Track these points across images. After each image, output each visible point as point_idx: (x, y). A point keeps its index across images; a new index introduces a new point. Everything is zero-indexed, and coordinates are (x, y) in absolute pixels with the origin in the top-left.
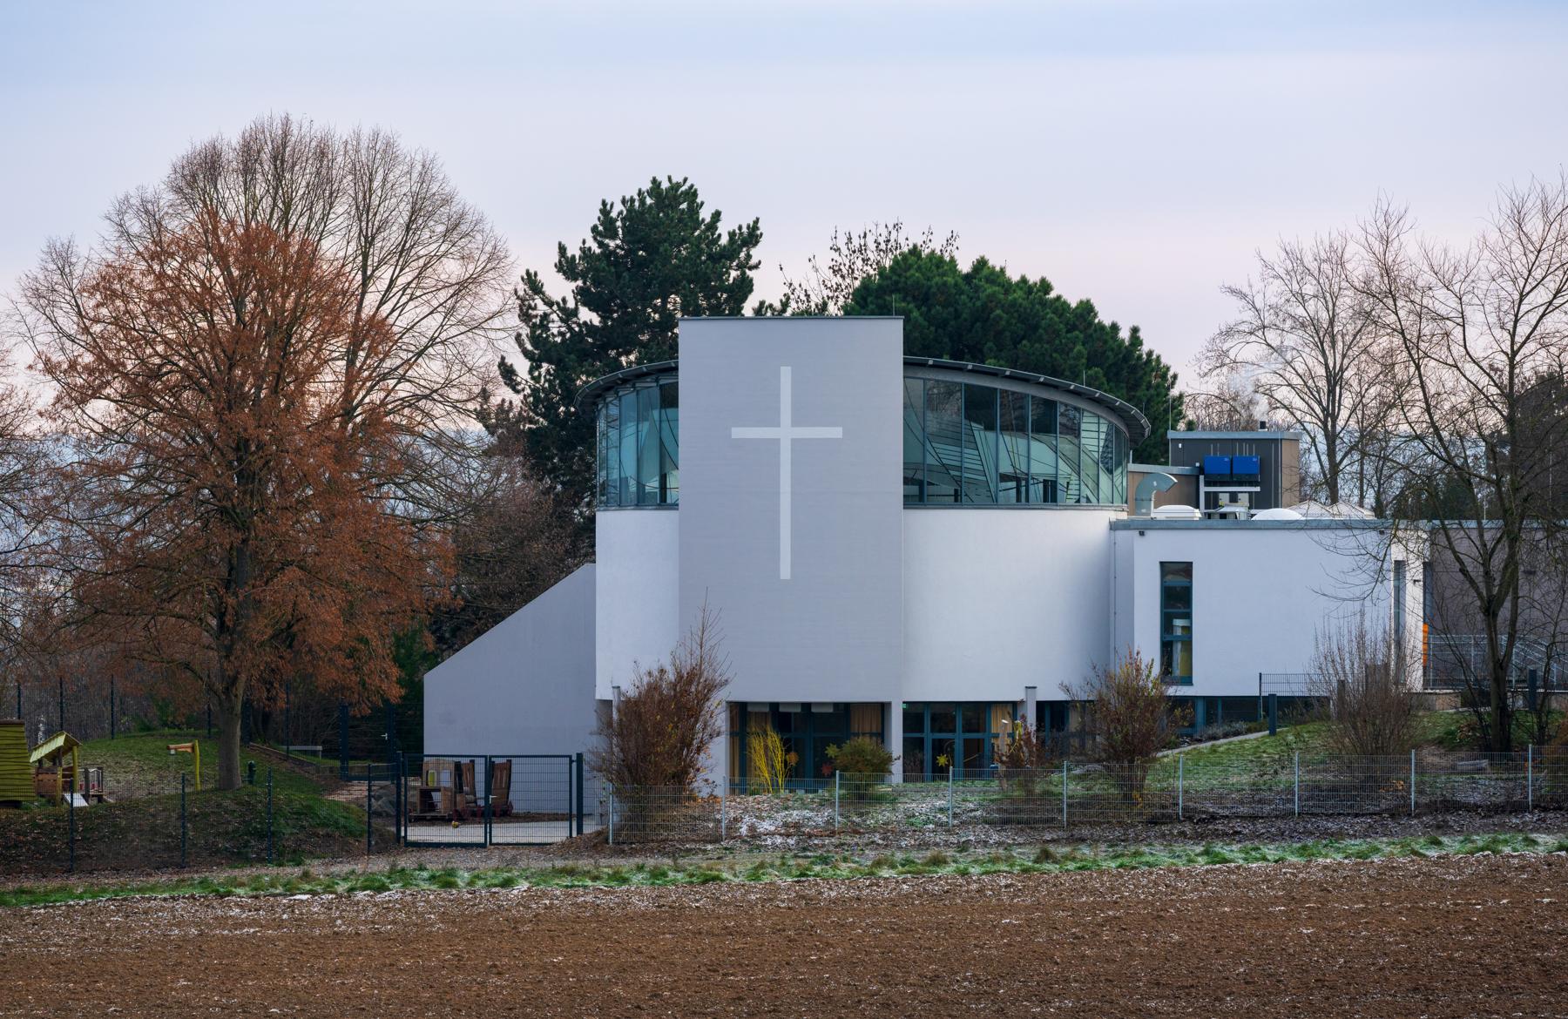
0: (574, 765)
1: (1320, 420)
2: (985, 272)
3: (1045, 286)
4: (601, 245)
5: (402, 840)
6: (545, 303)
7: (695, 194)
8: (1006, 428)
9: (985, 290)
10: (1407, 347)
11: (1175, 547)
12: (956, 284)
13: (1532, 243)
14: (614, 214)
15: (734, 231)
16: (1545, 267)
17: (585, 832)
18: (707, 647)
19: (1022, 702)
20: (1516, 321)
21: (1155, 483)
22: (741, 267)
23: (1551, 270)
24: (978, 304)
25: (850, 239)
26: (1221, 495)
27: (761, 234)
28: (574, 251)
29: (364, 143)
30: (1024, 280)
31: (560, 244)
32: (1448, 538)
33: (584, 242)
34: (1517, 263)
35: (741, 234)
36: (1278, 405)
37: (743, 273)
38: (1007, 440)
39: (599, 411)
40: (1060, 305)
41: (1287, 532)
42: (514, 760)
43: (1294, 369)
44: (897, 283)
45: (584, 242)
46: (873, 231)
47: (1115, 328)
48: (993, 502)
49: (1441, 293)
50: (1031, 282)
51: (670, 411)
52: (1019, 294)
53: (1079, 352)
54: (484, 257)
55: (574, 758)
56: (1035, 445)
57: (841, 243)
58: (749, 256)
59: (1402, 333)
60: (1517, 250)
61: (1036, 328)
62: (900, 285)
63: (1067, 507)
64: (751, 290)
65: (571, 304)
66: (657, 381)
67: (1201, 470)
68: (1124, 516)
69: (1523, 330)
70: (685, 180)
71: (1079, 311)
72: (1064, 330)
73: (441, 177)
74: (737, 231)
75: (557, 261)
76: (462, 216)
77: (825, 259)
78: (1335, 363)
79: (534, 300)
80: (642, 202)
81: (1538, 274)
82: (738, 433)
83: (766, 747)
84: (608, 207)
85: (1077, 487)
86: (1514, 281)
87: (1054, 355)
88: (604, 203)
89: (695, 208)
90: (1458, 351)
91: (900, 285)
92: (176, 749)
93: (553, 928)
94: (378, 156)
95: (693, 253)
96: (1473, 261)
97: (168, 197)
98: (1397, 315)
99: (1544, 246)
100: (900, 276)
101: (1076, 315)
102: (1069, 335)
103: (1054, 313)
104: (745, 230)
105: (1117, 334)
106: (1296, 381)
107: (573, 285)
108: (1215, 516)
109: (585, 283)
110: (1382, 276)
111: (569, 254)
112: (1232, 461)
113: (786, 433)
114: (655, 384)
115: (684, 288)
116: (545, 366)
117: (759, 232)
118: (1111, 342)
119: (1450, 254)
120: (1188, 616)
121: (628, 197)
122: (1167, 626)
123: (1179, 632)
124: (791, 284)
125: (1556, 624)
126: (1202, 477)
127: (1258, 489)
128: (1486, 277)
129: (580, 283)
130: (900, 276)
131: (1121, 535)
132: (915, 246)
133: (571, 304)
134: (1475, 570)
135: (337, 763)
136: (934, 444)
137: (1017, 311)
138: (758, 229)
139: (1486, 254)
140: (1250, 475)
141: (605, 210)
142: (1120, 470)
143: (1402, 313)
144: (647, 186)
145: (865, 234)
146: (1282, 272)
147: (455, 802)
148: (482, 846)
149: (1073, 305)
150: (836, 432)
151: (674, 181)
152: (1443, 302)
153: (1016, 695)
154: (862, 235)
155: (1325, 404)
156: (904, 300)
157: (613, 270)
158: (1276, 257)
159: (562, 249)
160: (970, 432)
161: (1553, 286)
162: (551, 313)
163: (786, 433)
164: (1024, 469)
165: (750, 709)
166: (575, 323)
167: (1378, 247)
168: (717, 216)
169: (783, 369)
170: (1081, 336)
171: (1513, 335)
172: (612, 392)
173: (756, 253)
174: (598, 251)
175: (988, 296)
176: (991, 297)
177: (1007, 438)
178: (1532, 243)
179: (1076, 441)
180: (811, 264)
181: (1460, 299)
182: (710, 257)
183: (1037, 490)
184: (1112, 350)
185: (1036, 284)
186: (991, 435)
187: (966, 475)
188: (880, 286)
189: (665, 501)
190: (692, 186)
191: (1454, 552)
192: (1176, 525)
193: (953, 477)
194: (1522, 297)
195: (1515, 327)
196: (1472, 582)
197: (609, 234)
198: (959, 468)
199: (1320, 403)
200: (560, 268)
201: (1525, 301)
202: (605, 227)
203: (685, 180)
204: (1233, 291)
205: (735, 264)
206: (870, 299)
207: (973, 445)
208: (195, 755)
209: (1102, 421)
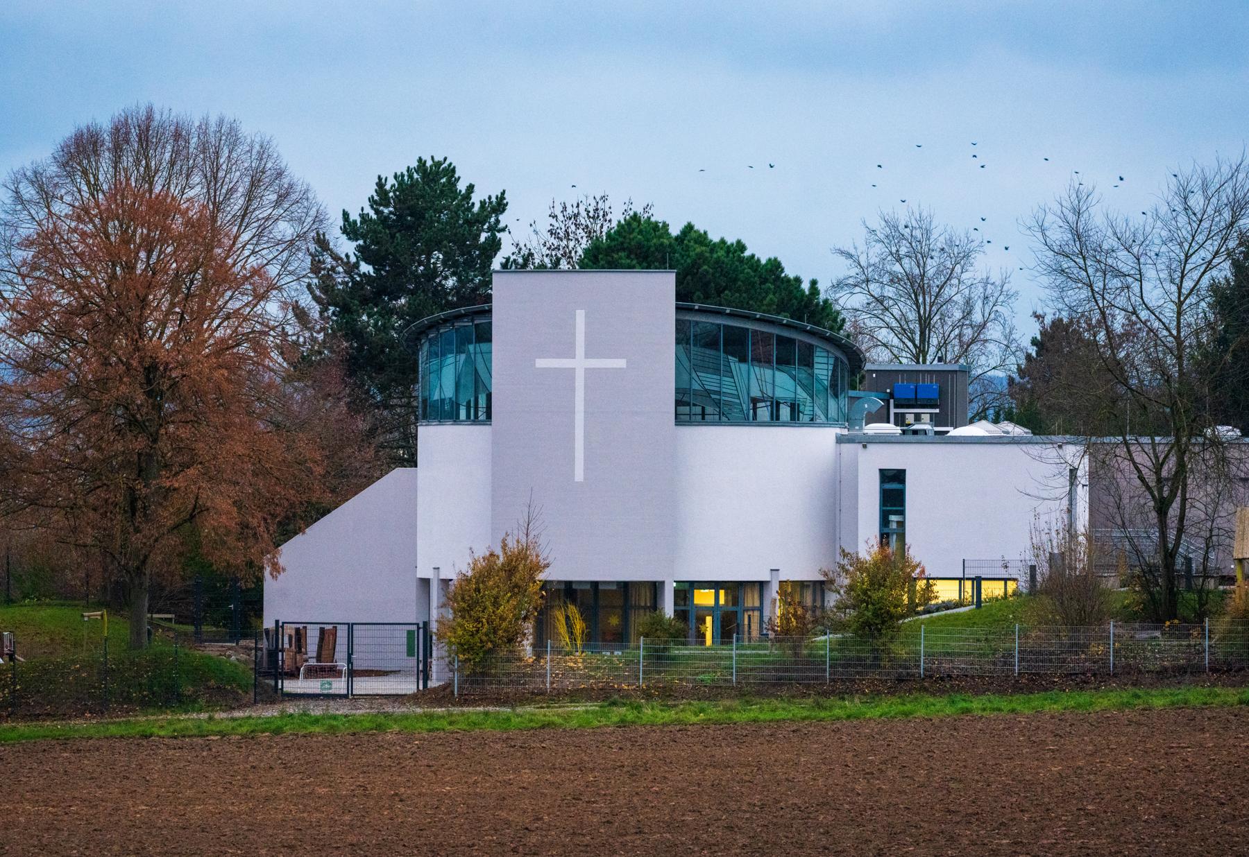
0: (421, 631)
1: (914, 357)
2: (693, 235)
3: (741, 247)
4: (377, 212)
5: (279, 692)
6: (332, 258)
7: (454, 170)
8: (757, 360)
9: (695, 249)
10: (1094, 298)
11: (892, 457)
12: (670, 245)
13: (1195, 214)
14: (388, 187)
15: (485, 200)
16: (1206, 233)
17: (429, 686)
18: (531, 536)
19: (768, 582)
20: (1182, 277)
21: (866, 406)
22: (490, 229)
23: (1211, 236)
24: (689, 261)
25: (565, 208)
26: (907, 416)
27: (507, 203)
28: (355, 216)
29: (213, 128)
30: (723, 241)
31: (344, 211)
32: (1129, 451)
33: (362, 209)
34: (1183, 230)
35: (491, 203)
36: (879, 343)
37: (494, 236)
38: (757, 371)
39: (422, 345)
40: (753, 261)
41: (999, 446)
42: (309, 626)
43: (892, 315)
44: (622, 243)
45: (362, 209)
46: (584, 202)
47: (798, 280)
48: (750, 419)
49: (1122, 254)
50: (729, 243)
51: (484, 346)
52: (721, 253)
53: (771, 299)
54: (309, 219)
55: (421, 625)
56: (778, 374)
57: (558, 211)
58: (498, 221)
59: (1091, 286)
60: (1182, 220)
61: (735, 280)
62: (625, 245)
63: (804, 425)
64: (499, 249)
65: (353, 259)
66: (472, 321)
67: (892, 395)
68: (845, 432)
69: (1188, 284)
70: (445, 159)
71: (769, 266)
72: (758, 282)
73: (275, 155)
74: (487, 200)
75: (342, 225)
76: (291, 186)
77: (544, 224)
78: (925, 309)
79: (323, 255)
80: (410, 176)
81: (1200, 238)
82: (542, 363)
83: (567, 618)
84: (383, 181)
85: (811, 409)
86: (1181, 244)
87: (751, 302)
88: (380, 178)
89: (453, 181)
90: (1135, 300)
91: (625, 245)
92: (89, 617)
93: (431, 764)
94: (224, 138)
95: (452, 218)
96: (1148, 229)
97: (53, 169)
98: (1086, 272)
99: (1205, 217)
100: (625, 237)
101: (766, 271)
102: (763, 286)
103: (749, 268)
104: (494, 199)
105: (799, 286)
106: (894, 324)
107: (355, 244)
108: (911, 435)
109: (365, 242)
110: (1075, 241)
111: (352, 218)
112: (916, 387)
113: (580, 363)
114: (471, 324)
115: (445, 247)
116: (332, 309)
117: (505, 202)
118: (795, 291)
119: (1131, 224)
120: (902, 513)
121: (399, 173)
122: (884, 521)
123: (894, 526)
124: (518, 245)
125: (1213, 522)
126: (892, 401)
127: (937, 411)
128: (1158, 241)
129: (361, 242)
130: (625, 237)
131: (846, 447)
132: (635, 214)
133: (353, 259)
134: (1151, 479)
135: (191, 628)
136: (699, 374)
137: (720, 267)
138: (504, 199)
139: (1159, 224)
140: (931, 399)
141: (380, 184)
142: (843, 395)
143: (1090, 271)
144: (414, 164)
145: (578, 204)
146: (882, 237)
147: (296, 659)
148: (345, 696)
149: (763, 261)
150: (621, 363)
151: (436, 159)
152: (1124, 261)
153: (765, 577)
154: (575, 205)
155: (917, 342)
156: (628, 257)
157: (388, 231)
158: (877, 224)
159: (346, 215)
160: (727, 364)
161: (1213, 249)
162: (337, 266)
163: (580, 363)
164: (771, 395)
165: (601, 587)
166: (357, 274)
167: (1072, 218)
168: (471, 188)
169: (578, 312)
170: (772, 287)
171: (1180, 289)
172: (434, 330)
173: (504, 219)
174: (374, 217)
175: (697, 254)
176: (700, 255)
177: (757, 369)
178: (1195, 214)
179: (810, 371)
180: (532, 229)
181: (1138, 260)
182: (467, 221)
183: (785, 412)
184: (796, 298)
185: (732, 245)
186: (744, 366)
187: (723, 398)
188: (609, 247)
189: (778, 418)
190: (451, 164)
191: (1135, 464)
192: (893, 440)
193: (713, 399)
194: (1187, 257)
195: (1182, 282)
196: (1148, 488)
197: (383, 202)
198: (719, 393)
199: (913, 341)
200: (344, 231)
201: (1190, 261)
202: (382, 196)
203: (445, 159)
204: (842, 253)
205: (485, 227)
206: (600, 256)
207: (730, 374)
208: (104, 621)
209: (830, 355)
